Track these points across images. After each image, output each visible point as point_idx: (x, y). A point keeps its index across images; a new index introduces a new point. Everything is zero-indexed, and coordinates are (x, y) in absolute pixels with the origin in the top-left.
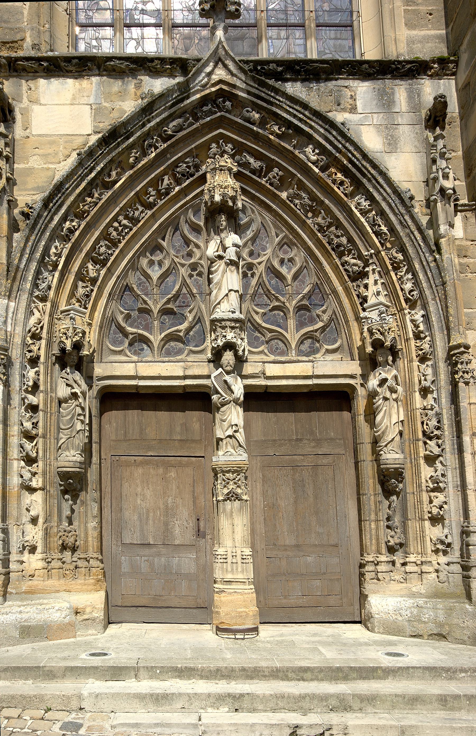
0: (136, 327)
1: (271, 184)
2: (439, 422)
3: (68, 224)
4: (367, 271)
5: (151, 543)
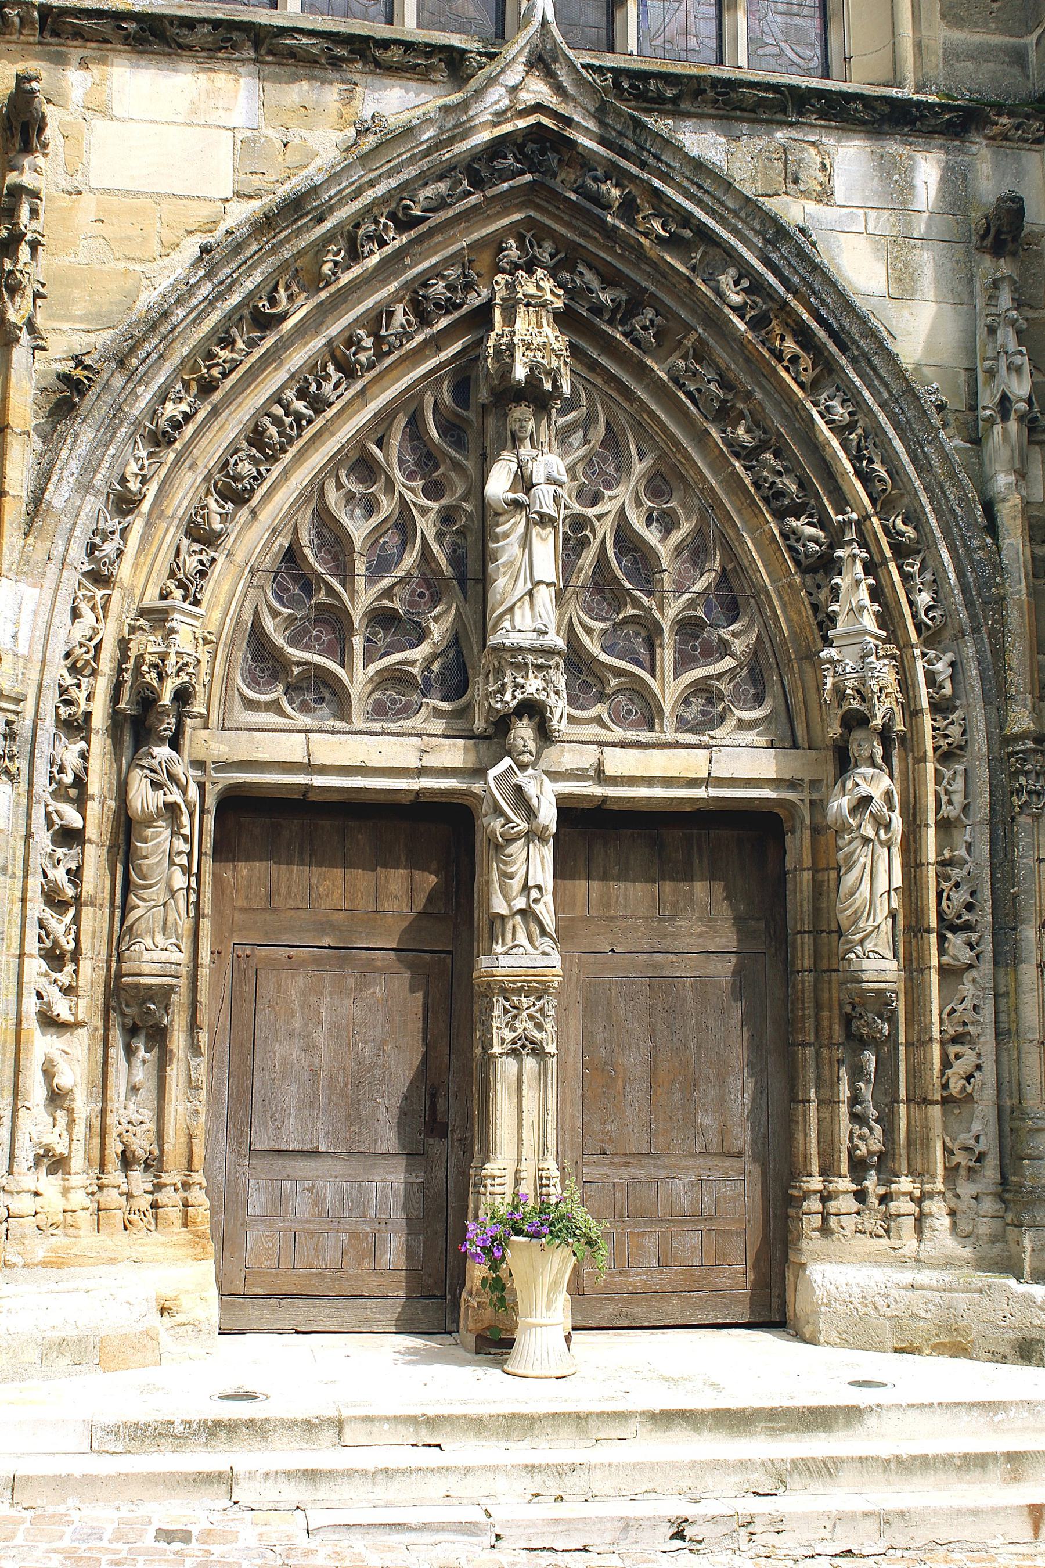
0: (308, 648)
1: (636, 342)
2: (972, 894)
3: (169, 406)
4: (839, 557)
5: (322, 1148)
